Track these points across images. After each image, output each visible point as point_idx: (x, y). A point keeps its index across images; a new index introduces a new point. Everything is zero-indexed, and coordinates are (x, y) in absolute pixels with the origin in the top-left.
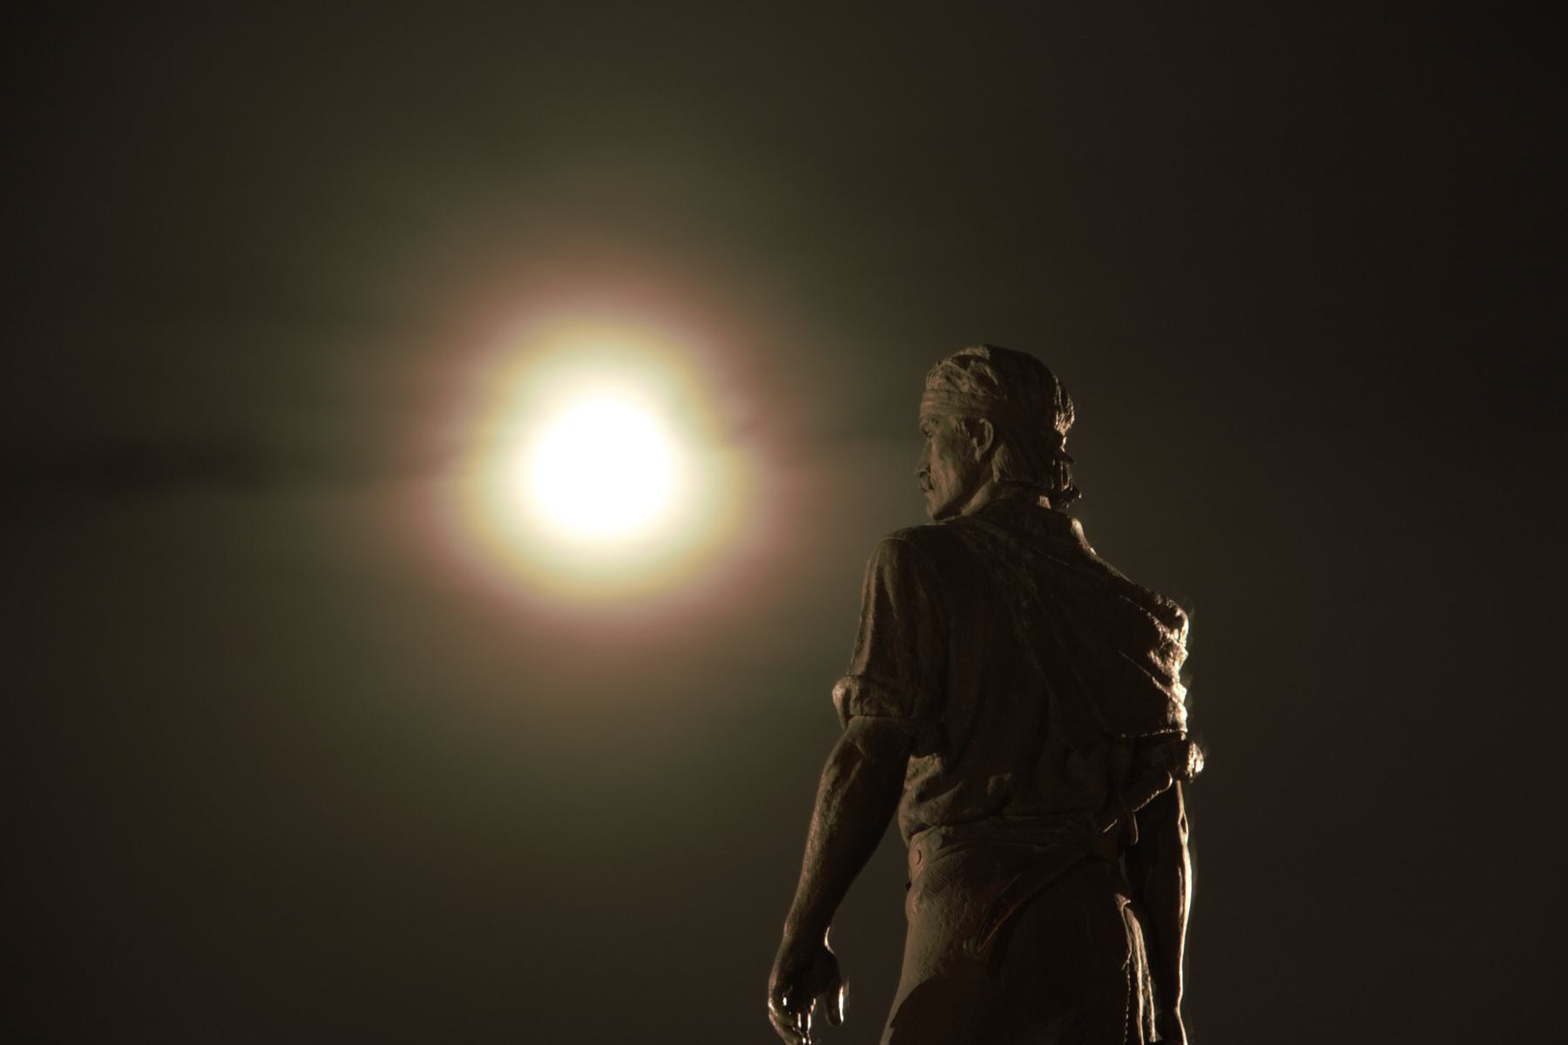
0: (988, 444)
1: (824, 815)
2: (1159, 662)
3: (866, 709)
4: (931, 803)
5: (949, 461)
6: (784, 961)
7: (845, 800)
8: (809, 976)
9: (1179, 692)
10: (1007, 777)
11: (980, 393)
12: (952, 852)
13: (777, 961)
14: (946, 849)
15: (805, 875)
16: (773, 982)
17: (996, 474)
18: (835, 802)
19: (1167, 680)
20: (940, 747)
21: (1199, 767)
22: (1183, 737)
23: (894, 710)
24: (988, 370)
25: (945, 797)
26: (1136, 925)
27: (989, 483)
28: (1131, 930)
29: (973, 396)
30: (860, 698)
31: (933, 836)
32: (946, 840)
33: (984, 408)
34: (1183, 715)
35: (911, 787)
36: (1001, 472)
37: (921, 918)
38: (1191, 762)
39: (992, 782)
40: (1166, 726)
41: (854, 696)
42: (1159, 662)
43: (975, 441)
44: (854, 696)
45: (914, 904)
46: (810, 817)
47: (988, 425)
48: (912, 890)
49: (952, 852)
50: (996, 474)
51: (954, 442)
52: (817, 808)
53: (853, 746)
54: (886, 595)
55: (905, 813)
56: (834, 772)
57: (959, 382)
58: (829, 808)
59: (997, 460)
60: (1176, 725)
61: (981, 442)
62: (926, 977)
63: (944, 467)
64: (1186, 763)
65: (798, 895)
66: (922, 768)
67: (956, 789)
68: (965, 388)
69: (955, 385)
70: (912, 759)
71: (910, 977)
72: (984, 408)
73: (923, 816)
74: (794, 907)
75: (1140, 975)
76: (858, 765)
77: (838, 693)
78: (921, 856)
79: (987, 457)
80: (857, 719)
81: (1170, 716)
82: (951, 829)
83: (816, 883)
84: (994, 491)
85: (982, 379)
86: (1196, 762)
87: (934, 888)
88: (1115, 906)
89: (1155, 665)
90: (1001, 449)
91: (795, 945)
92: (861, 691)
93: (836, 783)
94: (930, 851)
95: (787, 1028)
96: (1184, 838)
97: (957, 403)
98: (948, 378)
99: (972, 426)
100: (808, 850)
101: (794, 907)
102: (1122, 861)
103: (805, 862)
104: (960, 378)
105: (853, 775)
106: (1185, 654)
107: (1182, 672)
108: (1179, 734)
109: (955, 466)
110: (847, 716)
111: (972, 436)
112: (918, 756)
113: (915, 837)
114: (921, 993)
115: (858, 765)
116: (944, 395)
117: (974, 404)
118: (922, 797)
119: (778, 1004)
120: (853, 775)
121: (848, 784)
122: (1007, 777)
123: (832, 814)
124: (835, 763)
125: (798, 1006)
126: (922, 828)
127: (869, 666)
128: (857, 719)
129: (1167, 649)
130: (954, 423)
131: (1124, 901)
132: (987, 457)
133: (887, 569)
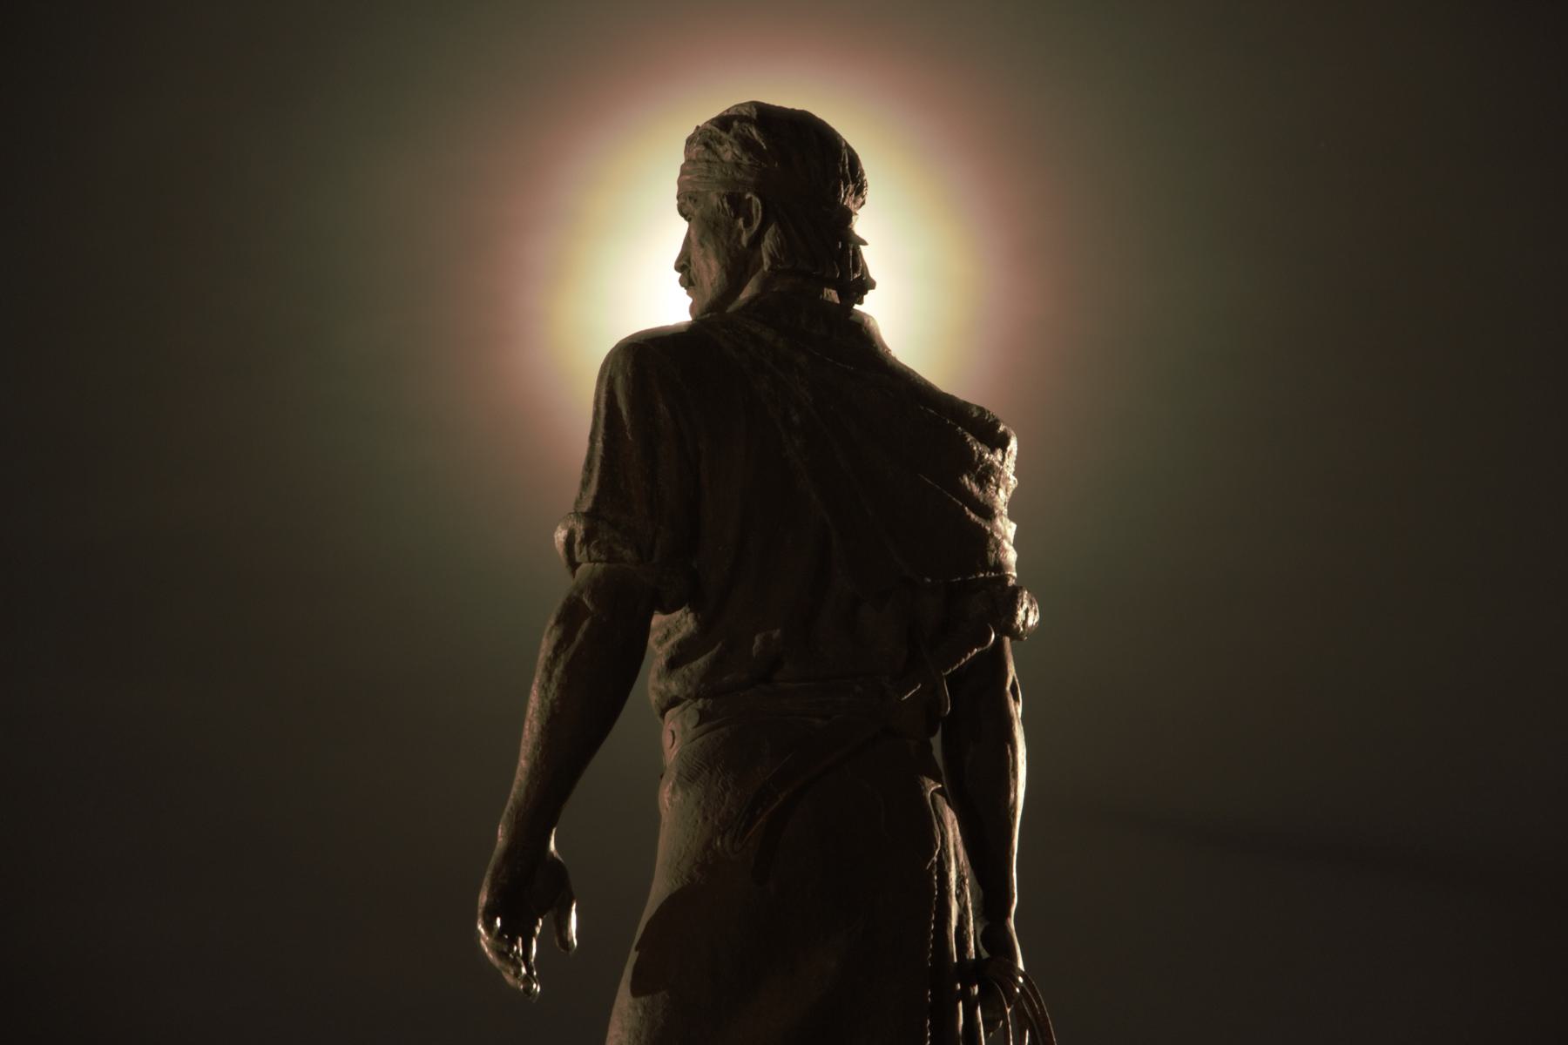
0: (756, 225)
1: (544, 689)
2: (976, 490)
3: (594, 553)
4: (684, 670)
5: (711, 249)
6: (497, 871)
7: (569, 668)
8: (529, 891)
9: (1007, 529)
10: (776, 634)
11: (745, 161)
12: (708, 731)
13: (489, 872)
14: (705, 726)
15: (523, 764)
16: (483, 899)
17: (766, 260)
18: (557, 671)
19: (988, 512)
20: (692, 598)
21: (1033, 620)
22: (1011, 582)
23: (628, 554)
24: (754, 132)
25: (700, 663)
26: (950, 816)
27: (759, 274)
28: (941, 821)
29: (738, 165)
30: (586, 540)
31: (688, 711)
32: (703, 716)
33: (751, 179)
34: (1011, 556)
35: (657, 652)
36: (772, 258)
37: (675, 818)
38: (1021, 613)
39: (758, 640)
40: (985, 567)
41: (578, 538)
42: (976, 490)
43: (741, 222)
44: (578, 538)
45: (667, 797)
46: (528, 692)
47: (756, 201)
48: (664, 781)
49: (708, 731)
50: (766, 260)
51: (716, 224)
52: (537, 681)
53: (579, 600)
54: (619, 410)
55: (652, 682)
56: (557, 633)
57: (721, 149)
58: (549, 679)
59: (768, 244)
60: (1000, 567)
61: (748, 223)
62: (678, 886)
63: (705, 256)
64: (1014, 614)
65: (514, 789)
66: (668, 628)
67: (714, 651)
68: (728, 156)
69: (715, 153)
70: (657, 619)
71: (660, 889)
72: (751, 179)
73: (674, 687)
74: (510, 803)
75: (953, 876)
76: (586, 624)
77: (560, 535)
78: (675, 737)
79: (756, 241)
80: (585, 568)
81: (992, 556)
82: (710, 702)
83: (535, 773)
84: (765, 284)
85: (747, 144)
86: (1028, 615)
87: (689, 777)
88: (919, 791)
89: (971, 493)
90: (772, 229)
91: (508, 854)
92: (587, 531)
93: (558, 648)
94: (685, 731)
95: (502, 955)
96: (1017, 710)
97: (718, 175)
98: (707, 145)
99: (736, 202)
100: (526, 733)
101: (510, 803)
102: (936, 741)
103: (523, 747)
104: (721, 144)
105: (579, 636)
106: (1013, 482)
107: (1011, 504)
108: (1005, 578)
109: (717, 256)
110: (573, 565)
111: (736, 217)
112: (666, 612)
113: (669, 714)
114: (672, 904)
115: (586, 624)
116: (703, 166)
117: (738, 176)
118: (673, 664)
119: (489, 926)
120: (579, 636)
121: (571, 650)
122: (776, 634)
123: (553, 686)
124: (558, 622)
125: (517, 927)
126: (674, 702)
127: (597, 499)
128: (585, 568)
129: (986, 475)
130: (715, 201)
131: (931, 786)
132: (756, 241)
133: (620, 380)
